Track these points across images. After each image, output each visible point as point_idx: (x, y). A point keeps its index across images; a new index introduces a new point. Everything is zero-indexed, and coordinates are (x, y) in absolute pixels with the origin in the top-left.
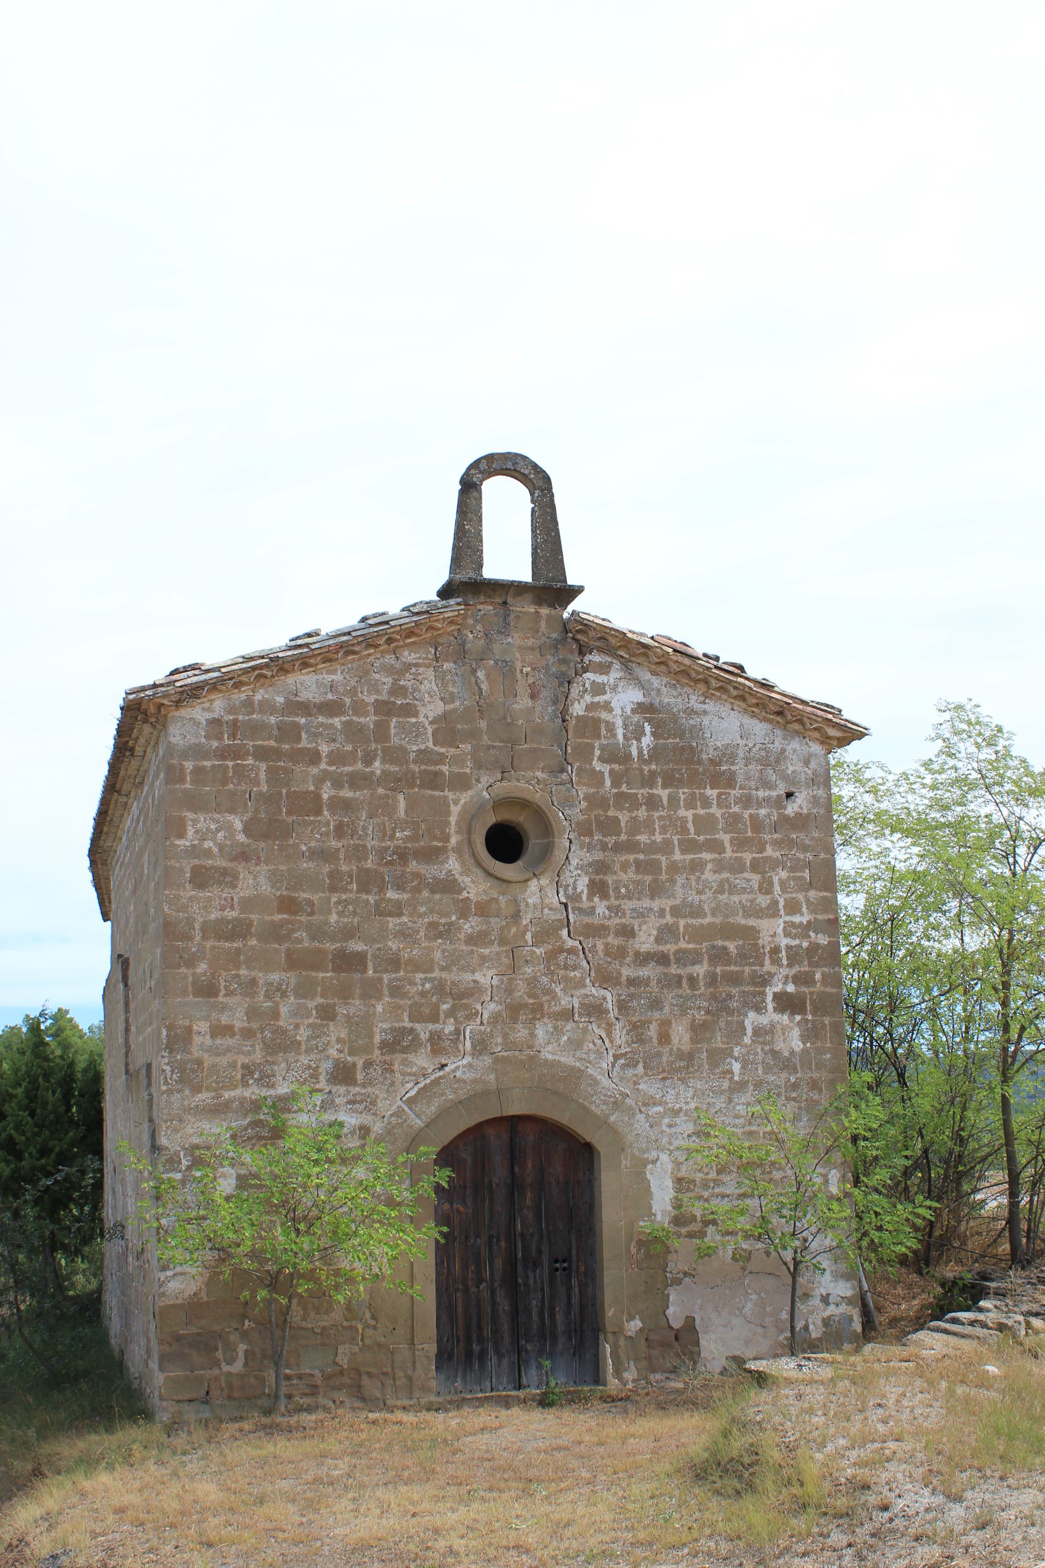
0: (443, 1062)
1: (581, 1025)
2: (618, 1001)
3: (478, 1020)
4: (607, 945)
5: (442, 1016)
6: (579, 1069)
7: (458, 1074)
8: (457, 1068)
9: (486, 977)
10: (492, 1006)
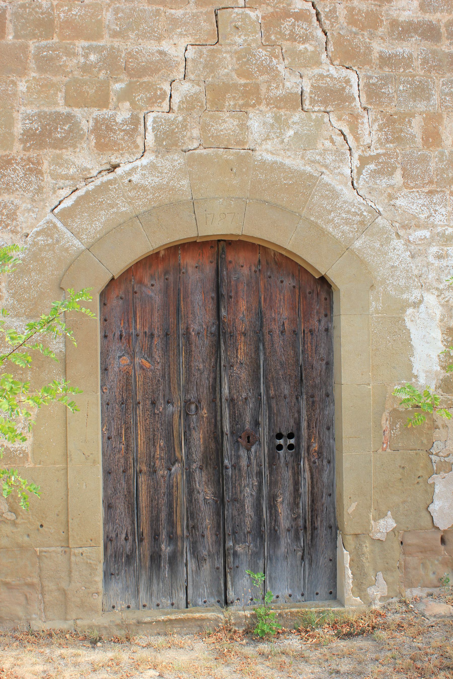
0: (114, 161)
1: (314, 116)
2: (367, 85)
3: (165, 106)
5: (113, 98)
7: (135, 178)
8: (134, 169)
9: (176, 47)
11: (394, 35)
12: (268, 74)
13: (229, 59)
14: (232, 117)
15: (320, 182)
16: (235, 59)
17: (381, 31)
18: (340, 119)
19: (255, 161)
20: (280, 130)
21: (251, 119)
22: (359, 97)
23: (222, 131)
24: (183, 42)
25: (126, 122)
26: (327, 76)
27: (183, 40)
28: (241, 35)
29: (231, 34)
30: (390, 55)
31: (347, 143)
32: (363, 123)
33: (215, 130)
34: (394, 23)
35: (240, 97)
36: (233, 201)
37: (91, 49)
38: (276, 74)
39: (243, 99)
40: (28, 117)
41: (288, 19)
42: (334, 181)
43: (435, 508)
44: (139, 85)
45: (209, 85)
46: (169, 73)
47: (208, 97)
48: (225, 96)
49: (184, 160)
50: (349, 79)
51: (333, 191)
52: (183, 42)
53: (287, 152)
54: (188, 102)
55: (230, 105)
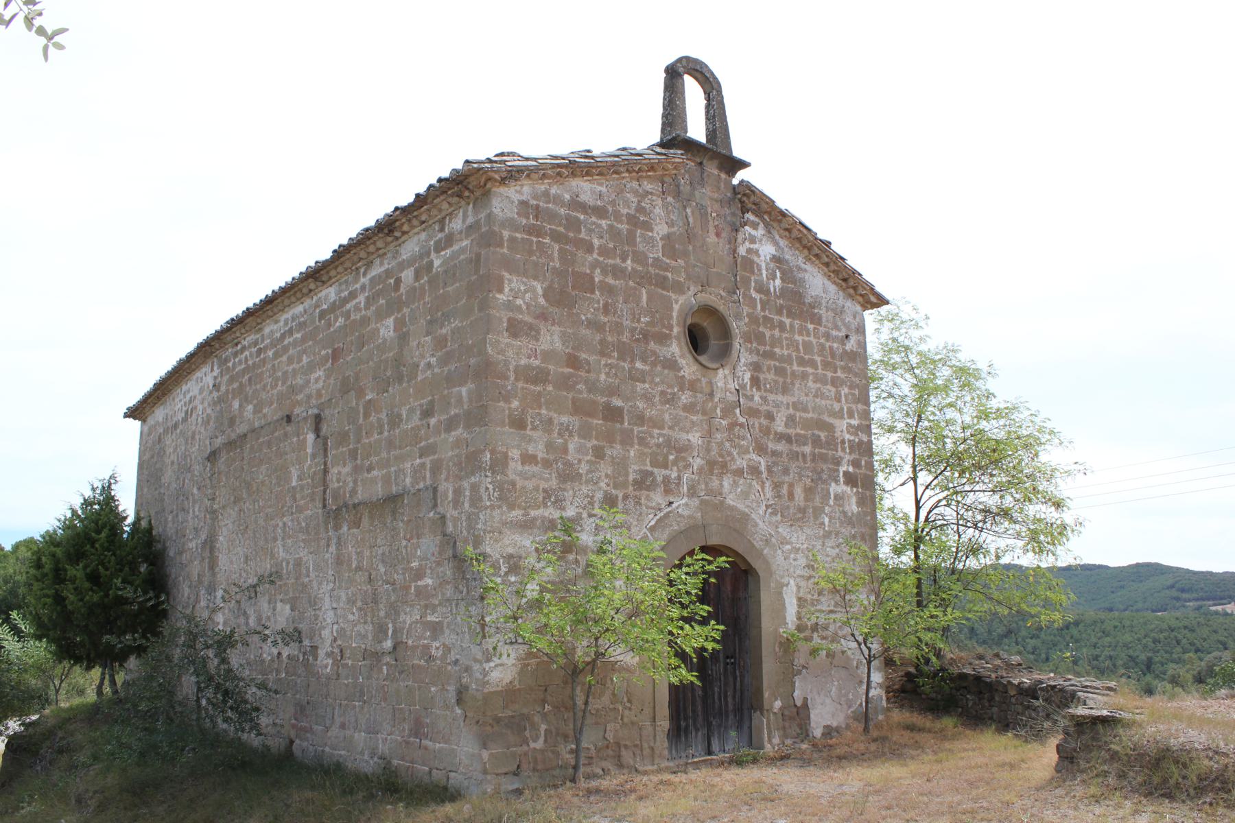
9: (695, 438)
34: (776, 433)
37: (660, 435)
40: (635, 471)
43: (795, 694)
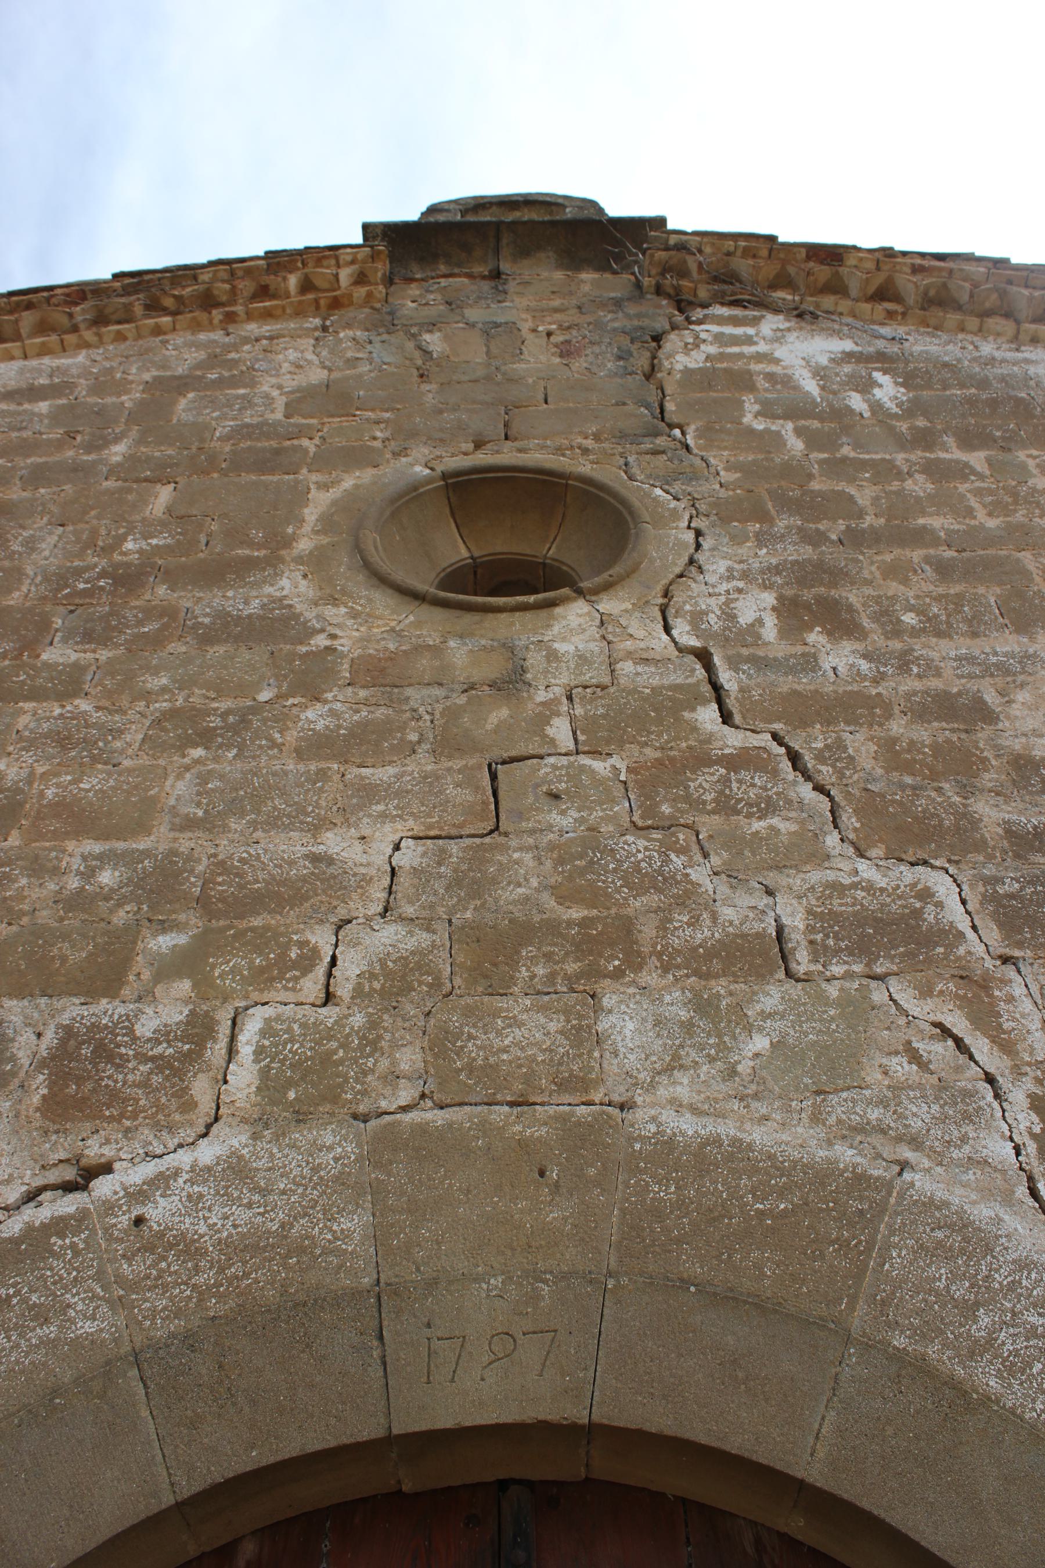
0: (95, 1150)
1: (833, 991)
2: (991, 899)
3: (312, 986)
4: (889, 745)
5: (142, 969)
6: (860, 1180)
7: (159, 1211)
8: (162, 1181)
9: (366, 846)
10: (388, 936)
11: (1034, 785)
12: (660, 891)
13: (531, 864)
14: (543, 1009)
15: (901, 1196)
16: (549, 864)
17: (988, 779)
18: (925, 992)
19: (631, 1139)
20: (719, 1036)
21: (610, 1011)
22: (974, 928)
23: (505, 1050)
24: (386, 835)
25: (168, 1033)
26: (855, 886)
27: (388, 828)
28: (568, 808)
29: (537, 809)
30: (1035, 827)
31: (971, 1057)
32: (1011, 999)
33: (479, 1048)
35: (567, 954)
36: (545, 1282)
38: (686, 891)
39: (577, 959)
41: (706, 770)
42: (959, 1191)
44: (234, 936)
45: (463, 927)
46: (335, 903)
47: (460, 959)
48: (518, 952)
49: (359, 1145)
50: (927, 889)
51: (962, 1225)
52: (386, 835)
53: (754, 1104)
54: (388, 974)
55: (533, 977)
